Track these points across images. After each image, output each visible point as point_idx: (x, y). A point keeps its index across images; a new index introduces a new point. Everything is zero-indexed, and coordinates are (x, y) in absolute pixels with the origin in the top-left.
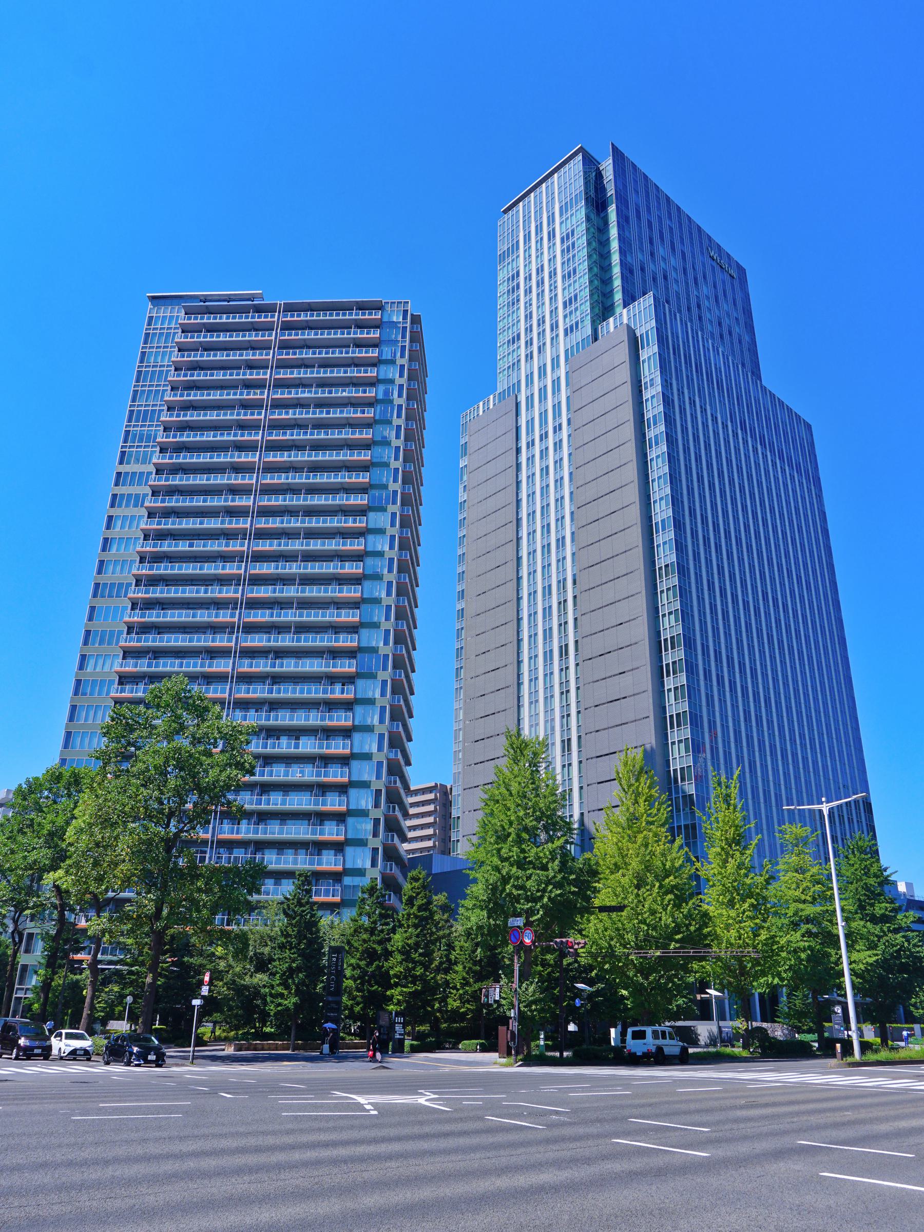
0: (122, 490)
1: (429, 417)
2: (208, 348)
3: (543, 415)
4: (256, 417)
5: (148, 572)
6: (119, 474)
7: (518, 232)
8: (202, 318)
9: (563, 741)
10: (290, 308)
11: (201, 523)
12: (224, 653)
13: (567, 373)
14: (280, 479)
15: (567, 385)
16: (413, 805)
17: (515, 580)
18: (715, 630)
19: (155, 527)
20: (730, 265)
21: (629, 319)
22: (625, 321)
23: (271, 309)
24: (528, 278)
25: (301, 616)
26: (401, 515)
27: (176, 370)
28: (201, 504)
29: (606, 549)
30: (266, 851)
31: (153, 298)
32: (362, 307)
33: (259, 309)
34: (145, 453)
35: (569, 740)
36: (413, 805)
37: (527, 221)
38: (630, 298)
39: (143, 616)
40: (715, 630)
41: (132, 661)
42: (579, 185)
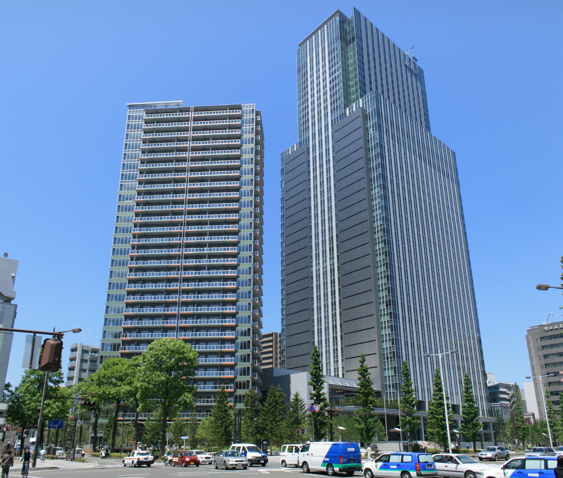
0: (122, 203)
1: (265, 257)
2: (158, 131)
3: (321, 154)
4: (187, 116)
5: (139, 232)
6: (129, 116)
7: (307, 57)
8: (154, 116)
9: (335, 369)
10: (196, 110)
11: (161, 219)
12: (176, 280)
13: (332, 133)
14: (200, 154)
15: (333, 138)
16: (264, 359)
17: (306, 152)
18: (400, 205)
19: (139, 221)
20: (415, 69)
21: (363, 104)
22: (361, 106)
23: (187, 110)
24: (313, 103)
25: (211, 239)
26: (256, 130)
27: (144, 143)
28: (163, 177)
29: (351, 201)
30: (199, 383)
31: (130, 106)
32: (232, 108)
33: (182, 110)
34: (135, 154)
35: (338, 368)
36: (264, 359)
37: (312, 50)
38: (363, 93)
39: (138, 252)
40: (400, 205)
41: (127, 347)
42: (336, 33)
